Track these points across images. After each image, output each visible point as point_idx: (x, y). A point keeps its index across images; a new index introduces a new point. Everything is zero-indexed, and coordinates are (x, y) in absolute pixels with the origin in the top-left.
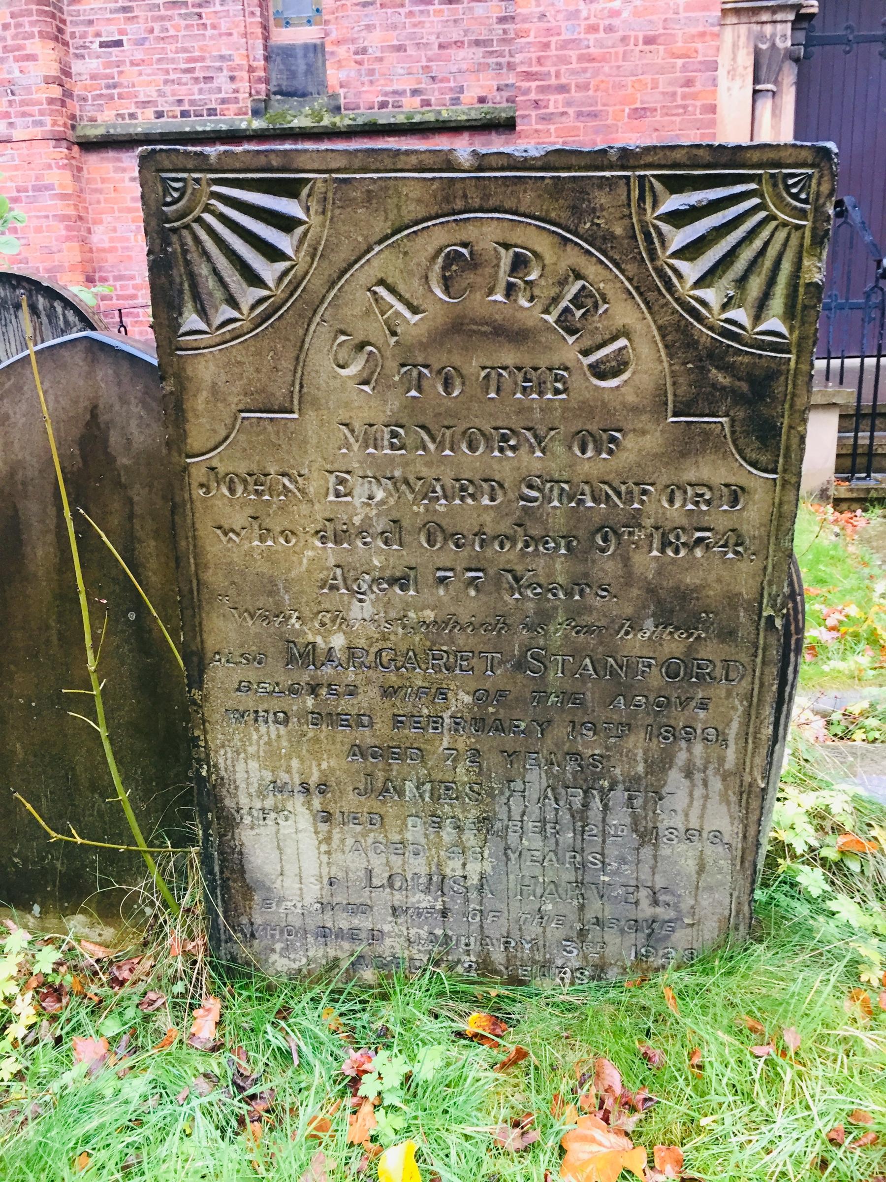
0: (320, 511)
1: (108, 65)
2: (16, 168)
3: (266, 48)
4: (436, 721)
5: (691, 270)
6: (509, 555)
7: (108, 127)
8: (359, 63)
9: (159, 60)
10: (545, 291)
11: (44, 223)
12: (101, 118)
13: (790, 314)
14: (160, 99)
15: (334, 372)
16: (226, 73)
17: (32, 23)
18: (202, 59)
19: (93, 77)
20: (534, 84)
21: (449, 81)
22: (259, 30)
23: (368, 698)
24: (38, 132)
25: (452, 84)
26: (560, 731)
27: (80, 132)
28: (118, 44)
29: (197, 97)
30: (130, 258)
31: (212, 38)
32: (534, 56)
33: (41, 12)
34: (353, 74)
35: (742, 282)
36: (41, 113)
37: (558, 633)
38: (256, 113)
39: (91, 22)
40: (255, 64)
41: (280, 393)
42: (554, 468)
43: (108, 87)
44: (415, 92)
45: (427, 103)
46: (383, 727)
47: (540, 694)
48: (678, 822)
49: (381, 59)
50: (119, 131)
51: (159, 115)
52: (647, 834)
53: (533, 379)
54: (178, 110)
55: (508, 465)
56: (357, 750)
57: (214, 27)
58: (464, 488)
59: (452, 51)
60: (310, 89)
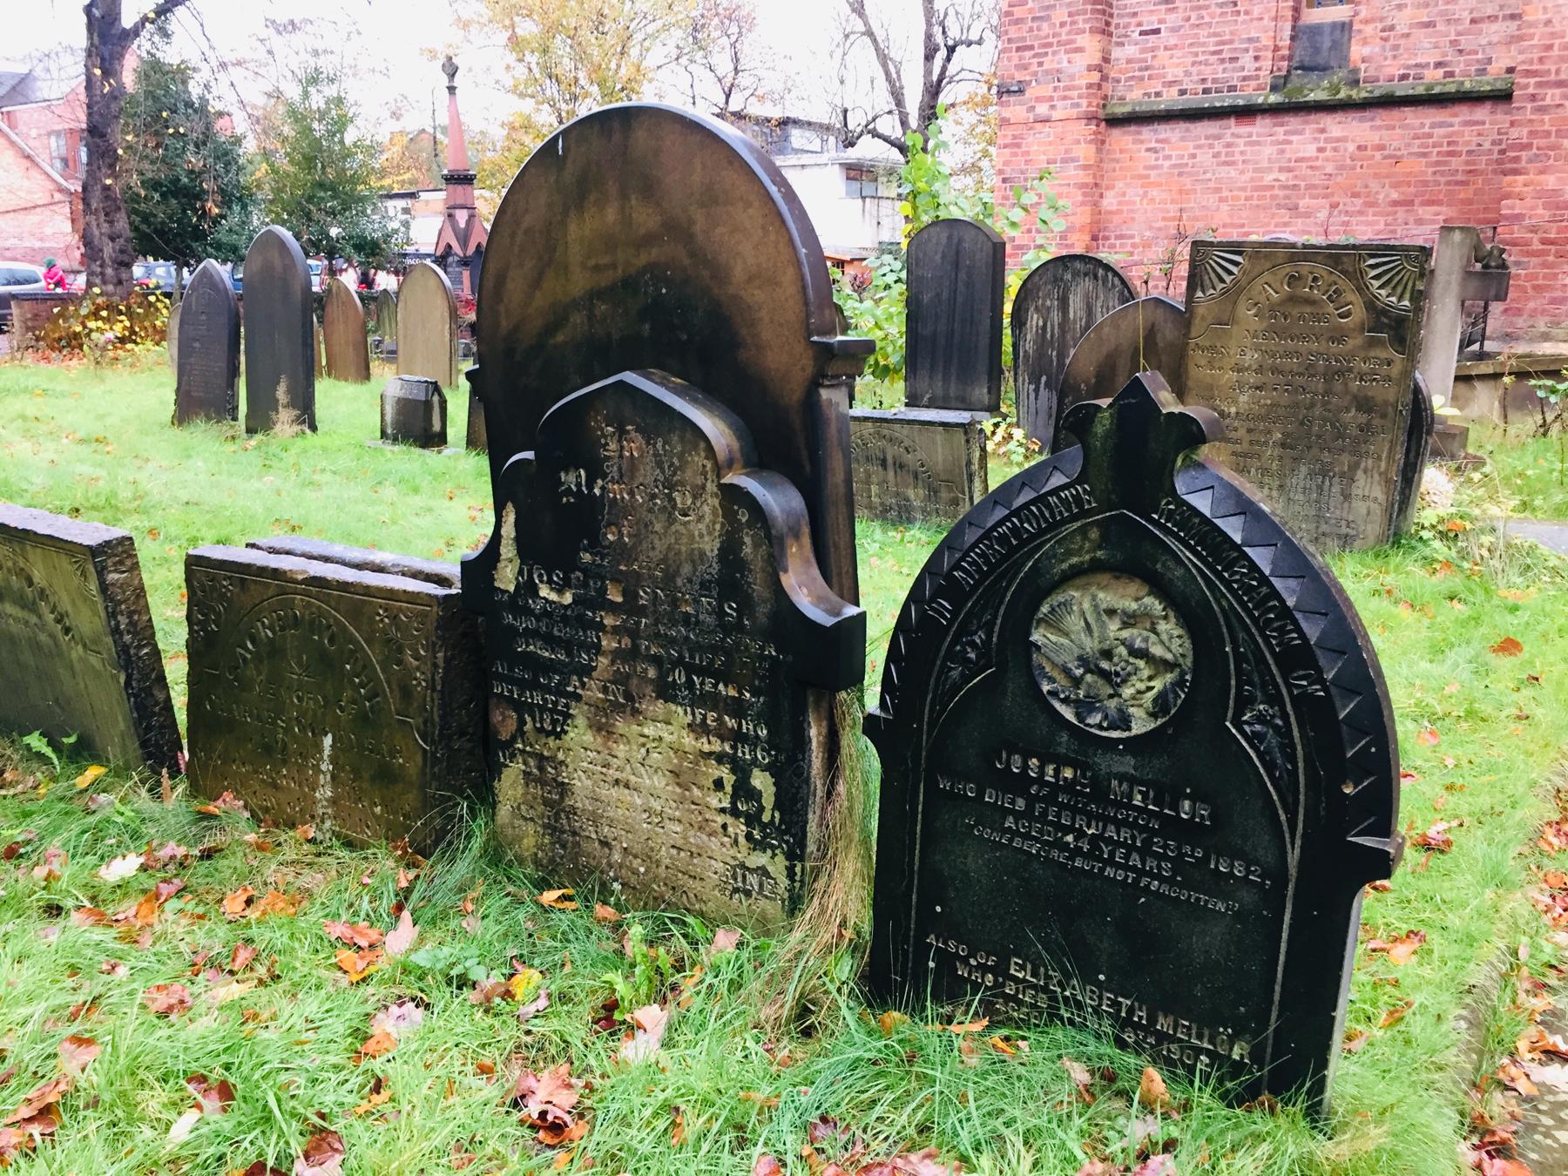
0: (1233, 361)
1: (1143, 51)
2: (1050, 143)
3: (1294, 28)
4: (1266, 443)
5: (1376, 283)
6: (1300, 380)
7: (1134, 104)
8: (1385, 39)
9: (1191, 45)
10: (1323, 289)
11: (1065, 190)
12: (1130, 96)
13: (1411, 300)
14: (1186, 80)
15: (1246, 313)
16: (1251, 53)
17: (1085, 21)
18: (1231, 42)
19: (1129, 61)
20: (1532, 81)
21: (1476, 53)
22: (1290, 13)
23: (1242, 432)
24: (1074, 112)
25: (1480, 56)
26: (1315, 451)
27: (1109, 110)
28: (1157, 31)
29: (1220, 76)
30: (1133, 219)
31: (1244, 22)
32: (1536, 56)
33: (1094, 11)
34: (1377, 49)
35: (1394, 288)
36: (1080, 97)
37: (1318, 411)
38: (1274, 88)
39: (1135, 14)
40: (1280, 44)
41: (1225, 318)
42: (1321, 350)
43: (1140, 70)
44: (1438, 65)
45: (1451, 74)
46: (1246, 445)
47: (1309, 433)
48: (1360, 492)
49: (1408, 35)
50: (1144, 108)
51: (1183, 92)
52: (1347, 497)
53: (1318, 317)
54: (1200, 87)
55: (1303, 346)
56: (1234, 453)
57: (1247, 13)
58: (1288, 354)
59: (1483, 26)
60: (1332, 63)
